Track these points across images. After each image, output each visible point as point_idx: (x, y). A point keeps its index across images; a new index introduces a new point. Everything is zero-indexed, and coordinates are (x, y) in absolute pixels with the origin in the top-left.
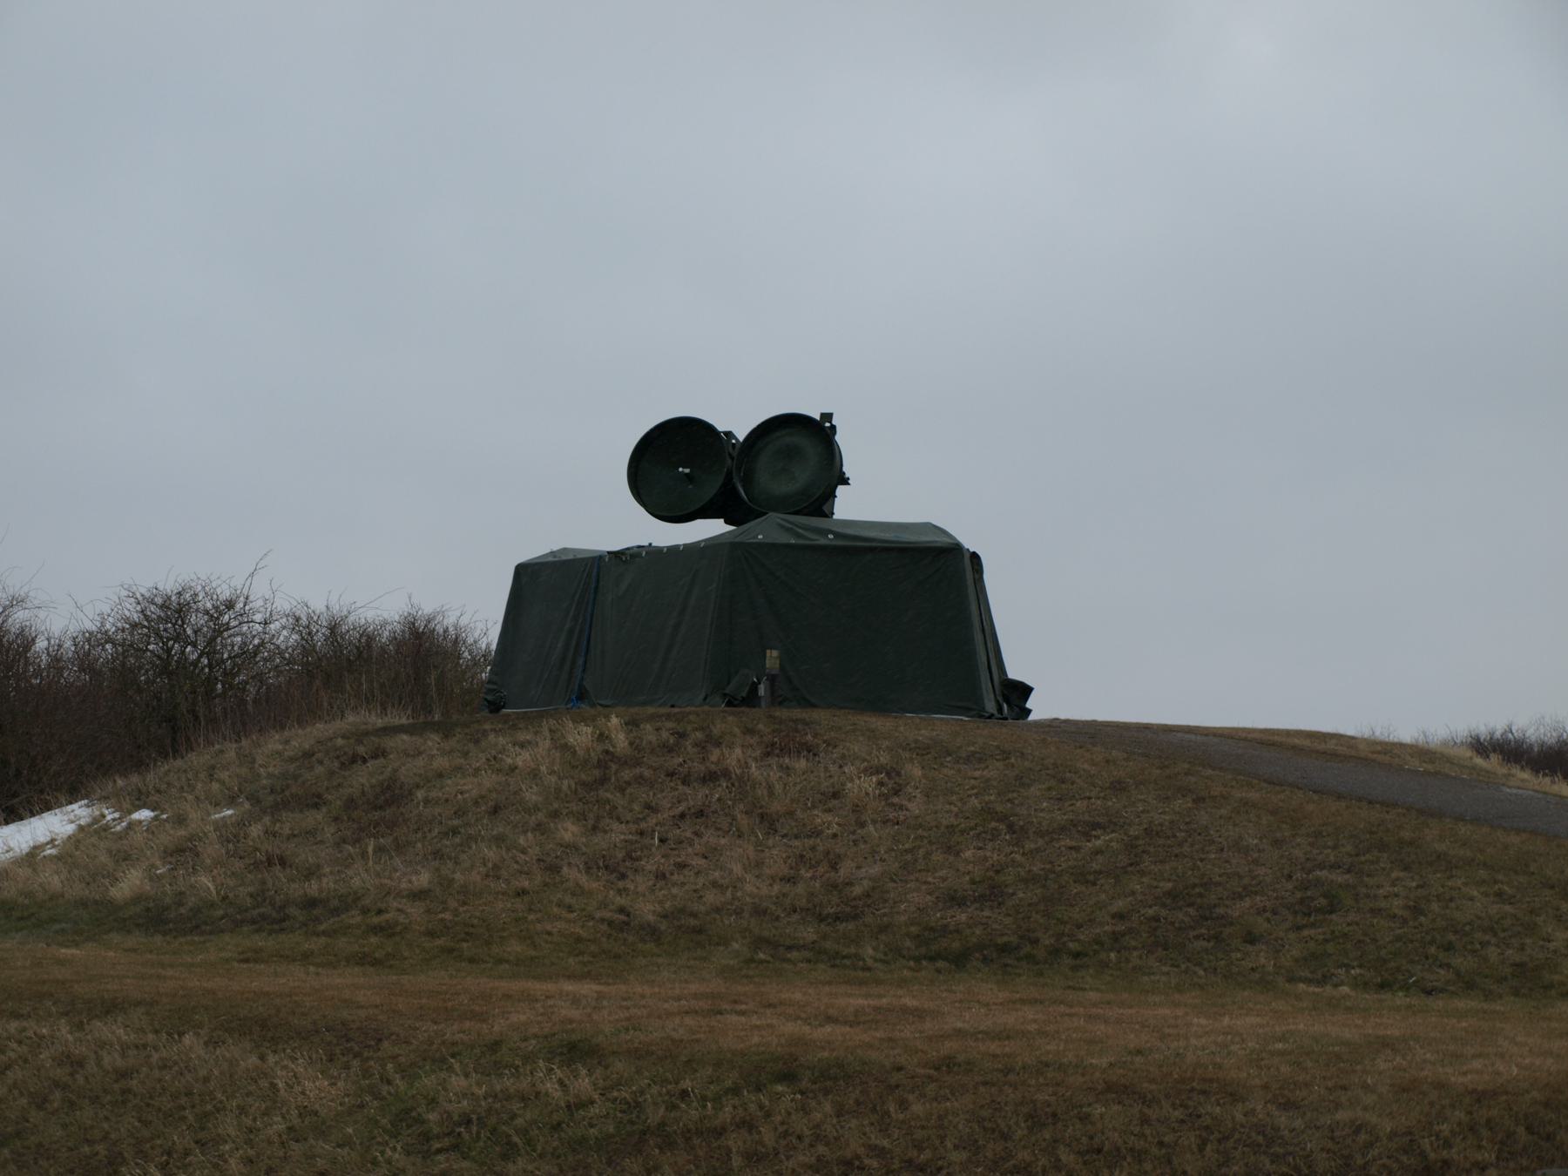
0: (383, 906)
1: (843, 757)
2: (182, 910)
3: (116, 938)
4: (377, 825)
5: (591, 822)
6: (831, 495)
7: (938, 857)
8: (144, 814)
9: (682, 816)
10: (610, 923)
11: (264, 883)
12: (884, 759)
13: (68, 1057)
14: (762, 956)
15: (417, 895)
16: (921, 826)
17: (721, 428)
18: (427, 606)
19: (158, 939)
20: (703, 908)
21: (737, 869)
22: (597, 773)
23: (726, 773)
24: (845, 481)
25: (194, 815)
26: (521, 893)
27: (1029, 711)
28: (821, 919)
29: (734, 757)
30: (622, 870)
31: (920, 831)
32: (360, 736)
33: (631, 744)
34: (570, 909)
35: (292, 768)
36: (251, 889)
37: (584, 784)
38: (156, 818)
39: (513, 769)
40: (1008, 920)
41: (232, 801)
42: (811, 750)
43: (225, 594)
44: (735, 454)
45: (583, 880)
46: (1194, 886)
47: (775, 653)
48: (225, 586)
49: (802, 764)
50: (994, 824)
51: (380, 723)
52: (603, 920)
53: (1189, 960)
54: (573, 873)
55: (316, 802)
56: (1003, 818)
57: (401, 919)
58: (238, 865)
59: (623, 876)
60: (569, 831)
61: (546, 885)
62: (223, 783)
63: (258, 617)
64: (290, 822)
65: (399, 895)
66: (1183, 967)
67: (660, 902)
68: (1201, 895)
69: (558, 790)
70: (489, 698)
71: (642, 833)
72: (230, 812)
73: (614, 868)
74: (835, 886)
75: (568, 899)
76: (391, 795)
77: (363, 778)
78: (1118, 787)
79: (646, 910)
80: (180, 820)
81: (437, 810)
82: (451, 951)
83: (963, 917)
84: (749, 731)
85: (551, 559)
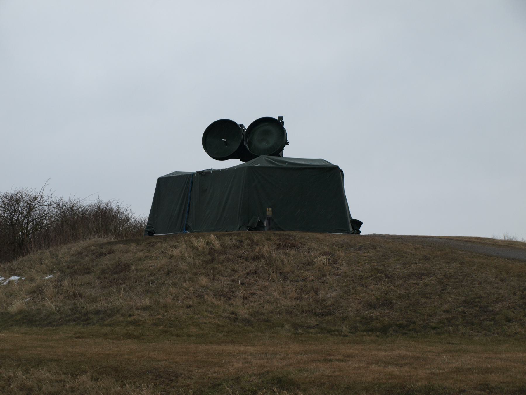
0: (131, 313)
1: (309, 249)
2: (42, 316)
3: (16, 328)
4: (117, 280)
5: (212, 277)
6: (282, 149)
7: (359, 288)
8: (15, 278)
9: (248, 274)
10: (230, 319)
11: (75, 304)
12: (326, 249)
13: (24, 386)
14: (300, 331)
15: (145, 308)
16: (348, 276)
17: (239, 123)
18: (105, 200)
19: (34, 328)
20: (266, 311)
21: (277, 295)
22: (209, 257)
23: (263, 256)
24: (287, 143)
25: (37, 277)
26: (189, 307)
27: (360, 232)
28: (316, 315)
29: (265, 249)
30: (229, 296)
31: (348, 278)
32: (101, 246)
33: (221, 245)
34: (211, 313)
35: (74, 258)
36: (70, 307)
37: (205, 262)
38: (19, 279)
39: (172, 256)
40: (398, 314)
41: (51, 272)
42: (294, 246)
43: (33, 194)
44: (244, 133)
45: (214, 301)
46: (475, 298)
47: (270, 209)
48: (33, 192)
49: (293, 252)
50: (379, 275)
51: (105, 241)
52: (226, 317)
53: (484, 330)
54: (210, 299)
55: (88, 271)
56: (382, 272)
57: (140, 318)
58: (62, 297)
59: (229, 299)
60: (204, 280)
61: (199, 303)
62: (46, 265)
63: (46, 203)
64: (80, 279)
65: (138, 309)
66: (483, 332)
67: (248, 309)
68: (479, 302)
69: (195, 264)
70: (149, 230)
71: (233, 281)
72: (51, 276)
73: (227, 296)
74: (318, 301)
75: (210, 309)
76: (122, 268)
77: (106, 262)
78: (426, 258)
79: (243, 312)
80: (32, 280)
81: (143, 273)
82: (166, 332)
83: (378, 313)
84: (269, 239)
85: (171, 175)
